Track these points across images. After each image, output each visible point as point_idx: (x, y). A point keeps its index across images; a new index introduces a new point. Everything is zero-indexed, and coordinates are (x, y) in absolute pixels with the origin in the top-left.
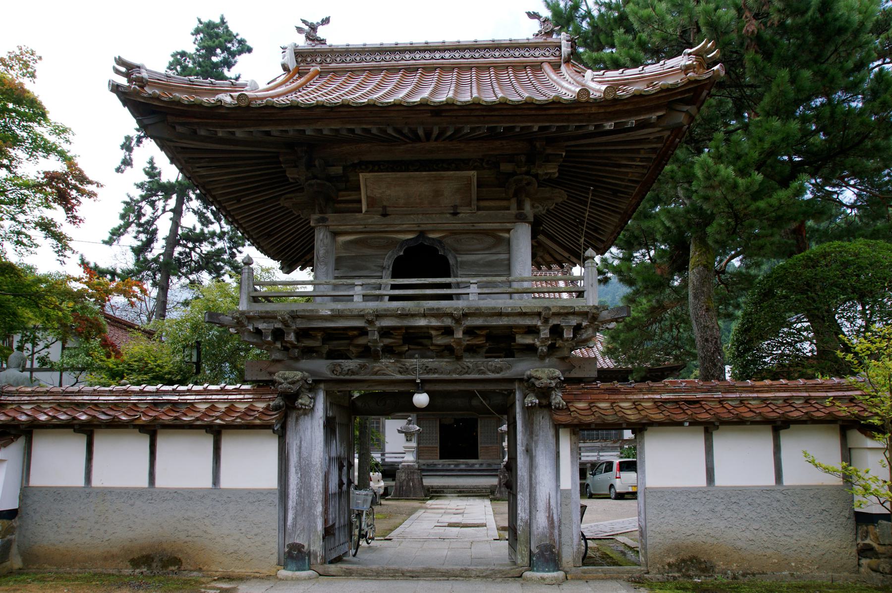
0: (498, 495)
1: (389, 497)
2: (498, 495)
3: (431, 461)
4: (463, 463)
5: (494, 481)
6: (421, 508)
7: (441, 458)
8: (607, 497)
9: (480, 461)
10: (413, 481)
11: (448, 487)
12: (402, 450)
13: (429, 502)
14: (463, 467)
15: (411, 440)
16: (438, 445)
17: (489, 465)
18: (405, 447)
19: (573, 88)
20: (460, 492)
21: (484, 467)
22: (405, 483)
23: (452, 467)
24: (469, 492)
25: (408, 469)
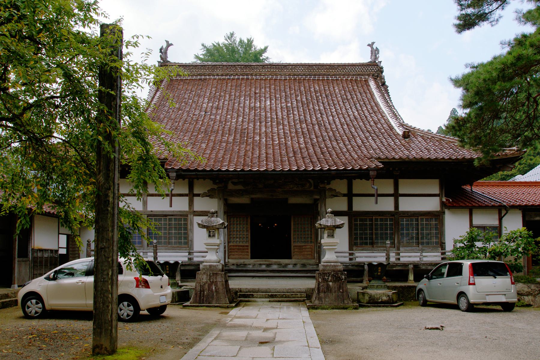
0: (317, 302)
1: (188, 303)
2: (317, 302)
3: (242, 261)
4: (275, 264)
5: (311, 284)
6: (217, 324)
7: (252, 258)
8: (455, 307)
9: (293, 261)
10: (216, 285)
11: (258, 291)
12: (206, 250)
13: (234, 312)
14: (275, 267)
15: (214, 236)
16: (249, 244)
17: (304, 265)
18: (207, 244)
19: (300, 162)
20: (272, 296)
21: (298, 268)
22: (206, 286)
23: (264, 267)
24: (282, 297)
25: (212, 271)
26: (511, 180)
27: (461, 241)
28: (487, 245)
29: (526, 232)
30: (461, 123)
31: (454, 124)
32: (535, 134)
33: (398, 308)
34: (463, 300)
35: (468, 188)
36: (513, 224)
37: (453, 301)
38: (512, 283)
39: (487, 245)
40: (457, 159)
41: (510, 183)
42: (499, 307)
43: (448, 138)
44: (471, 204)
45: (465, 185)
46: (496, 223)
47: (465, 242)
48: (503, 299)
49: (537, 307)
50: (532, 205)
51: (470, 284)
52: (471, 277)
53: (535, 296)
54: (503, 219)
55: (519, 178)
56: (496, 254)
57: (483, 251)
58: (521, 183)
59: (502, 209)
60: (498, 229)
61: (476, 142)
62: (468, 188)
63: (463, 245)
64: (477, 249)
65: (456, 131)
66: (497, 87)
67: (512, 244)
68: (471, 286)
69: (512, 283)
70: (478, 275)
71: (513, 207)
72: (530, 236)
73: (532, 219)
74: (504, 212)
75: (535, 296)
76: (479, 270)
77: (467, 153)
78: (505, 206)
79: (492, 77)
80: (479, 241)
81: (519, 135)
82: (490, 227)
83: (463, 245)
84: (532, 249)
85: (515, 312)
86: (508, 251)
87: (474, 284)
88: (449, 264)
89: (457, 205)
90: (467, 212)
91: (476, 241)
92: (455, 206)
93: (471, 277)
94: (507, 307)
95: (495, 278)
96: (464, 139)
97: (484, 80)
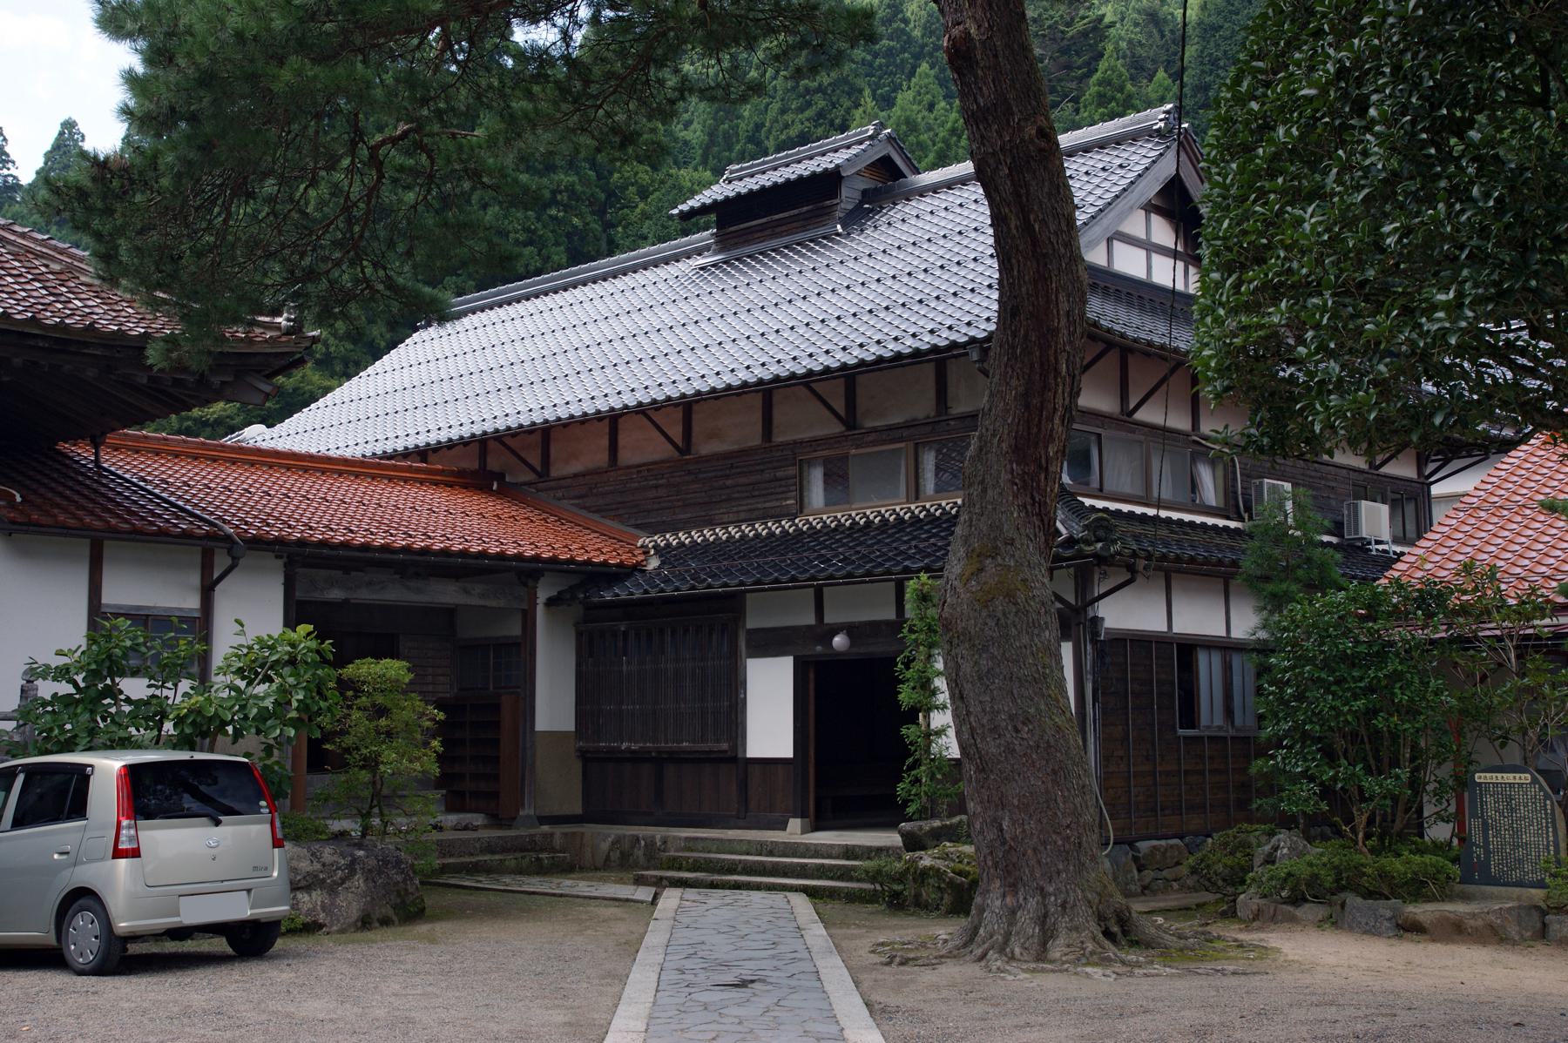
8: (48, 958)
26: (228, 440)
27: (62, 673)
28: (166, 692)
29: (313, 644)
30: (116, 183)
31: (87, 183)
32: (366, 280)
33: (857, 907)
34: (84, 924)
35: (83, 453)
36: (251, 616)
37: (38, 933)
38: (277, 843)
39: (166, 692)
40: (61, 327)
41: (232, 449)
42: (220, 945)
43: (23, 235)
44: (100, 518)
45: (74, 438)
46: (192, 603)
47: (79, 679)
48: (237, 909)
49: (342, 931)
50: (323, 544)
51: (118, 854)
52: (125, 823)
53: (332, 890)
54: (217, 588)
55: (256, 435)
56: (199, 728)
57: (151, 713)
58: (259, 452)
59: (215, 551)
60: (202, 624)
61: (157, 274)
62: (83, 453)
63: (70, 689)
64: (127, 708)
65: (90, 210)
66: (286, 75)
67: (261, 689)
68: (123, 861)
69: (277, 843)
70: (149, 816)
71: (259, 544)
72: (325, 661)
73: (317, 596)
74: (221, 562)
75: (332, 890)
76: (150, 794)
77: (120, 314)
78: (228, 538)
79: (268, 30)
80: (135, 673)
81: (311, 275)
82: (182, 619)
83: (70, 689)
84: (329, 709)
85: (277, 957)
86: (246, 718)
87: (135, 853)
88: (31, 771)
89: (45, 520)
90: (84, 548)
91: (123, 675)
92: (30, 523)
93: (125, 823)
94: (249, 941)
95: (218, 823)
96: (116, 248)
97: (239, 36)
